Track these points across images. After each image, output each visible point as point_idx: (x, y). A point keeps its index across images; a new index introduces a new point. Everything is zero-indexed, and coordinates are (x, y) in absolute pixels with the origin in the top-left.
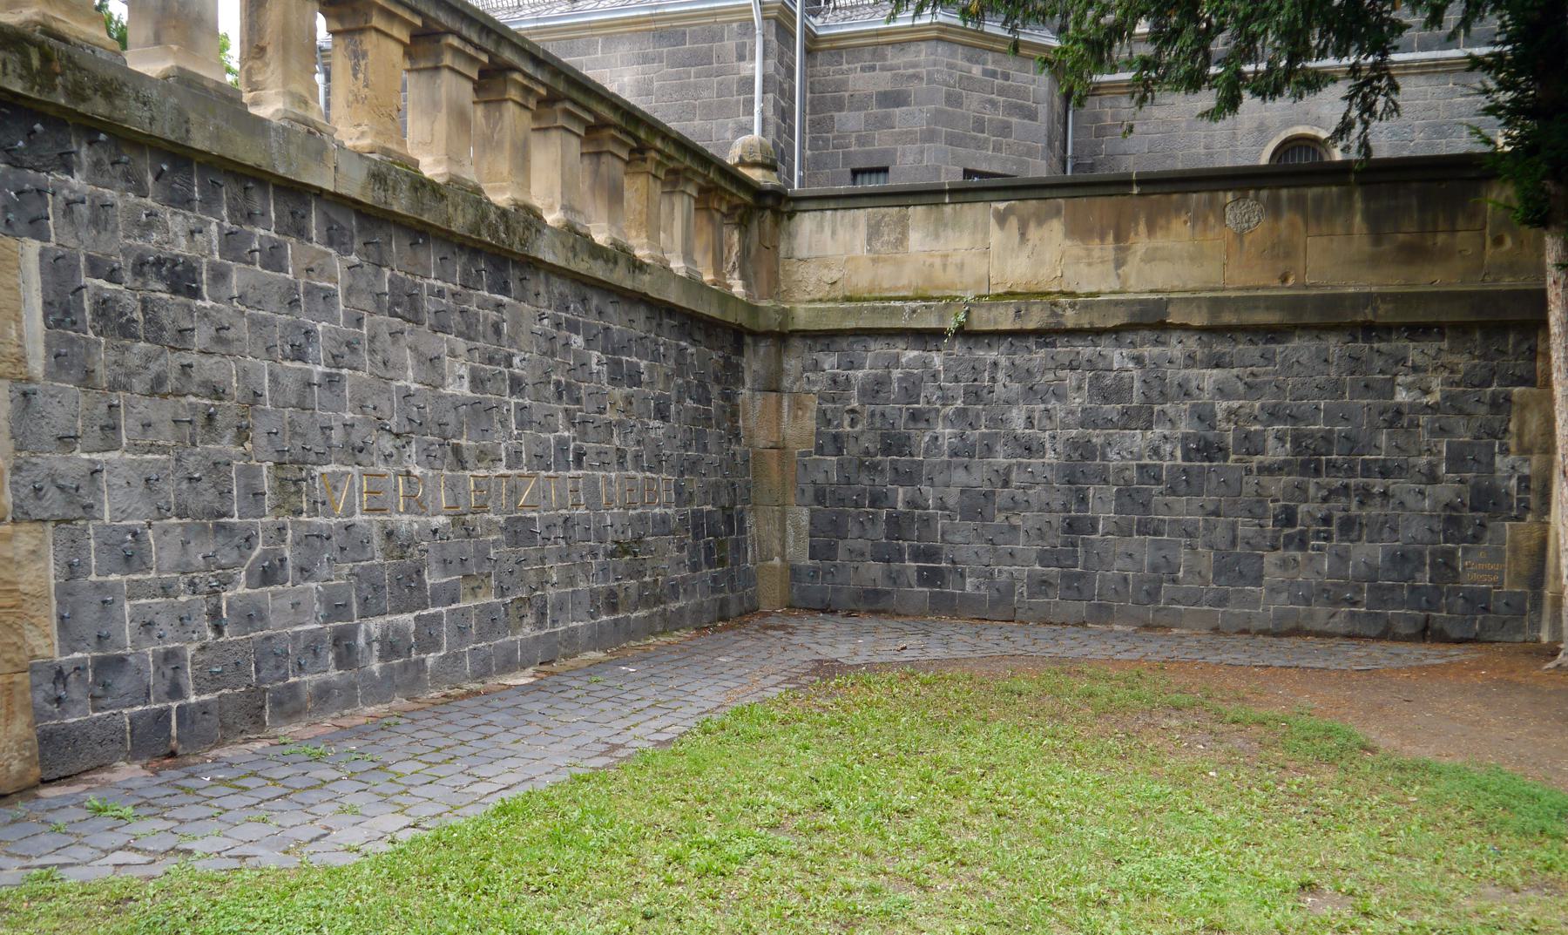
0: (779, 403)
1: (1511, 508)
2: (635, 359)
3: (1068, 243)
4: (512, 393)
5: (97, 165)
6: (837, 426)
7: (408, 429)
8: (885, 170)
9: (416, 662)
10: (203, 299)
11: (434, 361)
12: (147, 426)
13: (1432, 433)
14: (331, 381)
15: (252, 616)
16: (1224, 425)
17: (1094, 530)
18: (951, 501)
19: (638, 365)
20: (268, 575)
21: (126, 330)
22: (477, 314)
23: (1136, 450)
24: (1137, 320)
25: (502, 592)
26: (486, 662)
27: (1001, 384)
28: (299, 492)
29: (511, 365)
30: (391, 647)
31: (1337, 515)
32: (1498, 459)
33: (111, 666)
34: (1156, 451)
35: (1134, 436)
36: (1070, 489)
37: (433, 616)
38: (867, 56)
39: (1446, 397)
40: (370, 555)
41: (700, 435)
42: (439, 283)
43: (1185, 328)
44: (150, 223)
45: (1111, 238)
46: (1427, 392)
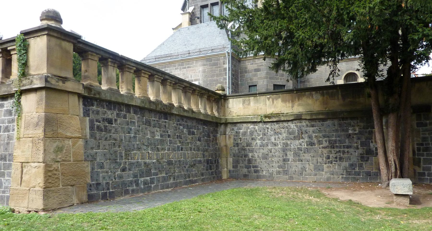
0: (226, 137)
1: (374, 154)
2: (194, 130)
3: (282, 103)
4: (168, 137)
5: (97, 105)
6: (237, 141)
7: (148, 145)
8: (256, 85)
9: (150, 186)
10: (113, 124)
11: (153, 133)
12: (104, 146)
13: (357, 139)
14: (135, 137)
15: (121, 177)
16: (314, 139)
17: (289, 161)
18: (260, 156)
19: (194, 131)
20: (124, 170)
21: (101, 130)
22: (161, 124)
23: (297, 144)
24: (296, 118)
25: (166, 174)
26: (163, 187)
27: (269, 132)
28: (129, 156)
29: (168, 133)
30: (145, 183)
31: (338, 156)
32: (371, 144)
33: (98, 184)
34: (301, 145)
35: (296, 142)
36: (284, 153)
37: (153, 178)
38: (252, 62)
39: (359, 132)
40: (141, 167)
41: (208, 144)
42: (154, 119)
43: (305, 119)
44: (105, 113)
45: (291, 102)
46: (355, 131)
